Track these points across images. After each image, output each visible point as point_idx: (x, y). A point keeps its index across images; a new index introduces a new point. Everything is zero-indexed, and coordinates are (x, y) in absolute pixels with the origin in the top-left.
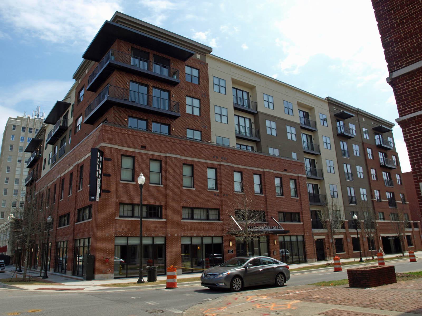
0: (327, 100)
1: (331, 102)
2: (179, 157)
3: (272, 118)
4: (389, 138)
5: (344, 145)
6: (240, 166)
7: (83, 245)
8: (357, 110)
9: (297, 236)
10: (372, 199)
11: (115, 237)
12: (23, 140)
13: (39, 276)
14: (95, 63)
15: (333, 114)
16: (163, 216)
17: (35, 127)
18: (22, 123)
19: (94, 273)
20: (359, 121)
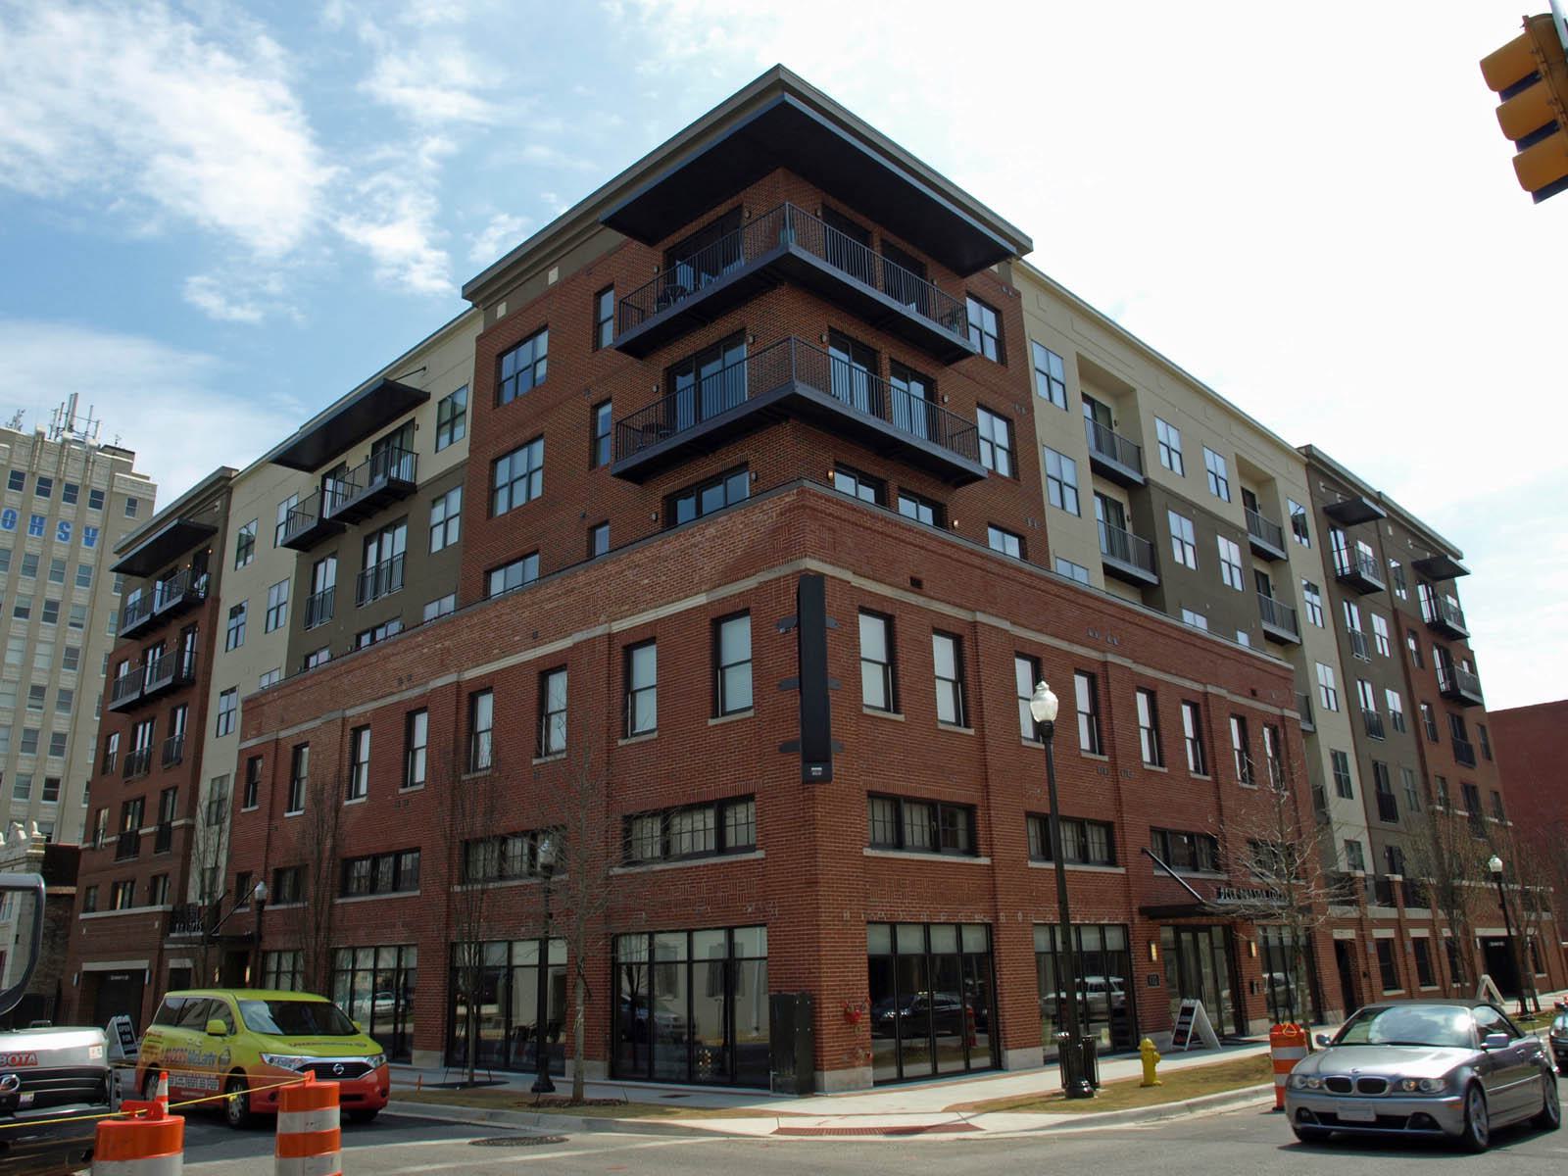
0: (1307, 456)
1: (1314, 464)
2: (1006, 625)
3: (1187, 508)
4: (1449, 597)
5: (1353, 613)
6: (1149, 672)
7: (685, 958)
8: (1376, 496)
9: (927, 927)
10: (1431, 807)
11: (869, 922)
12: (12, 523)
13: (895, 1076)
14: (622, 247)
15: (1320, 506)
16: (982, 848)
17: (65, 475)
18: (11, 456)
19: (816, 1066)
20: (1379, 536)
